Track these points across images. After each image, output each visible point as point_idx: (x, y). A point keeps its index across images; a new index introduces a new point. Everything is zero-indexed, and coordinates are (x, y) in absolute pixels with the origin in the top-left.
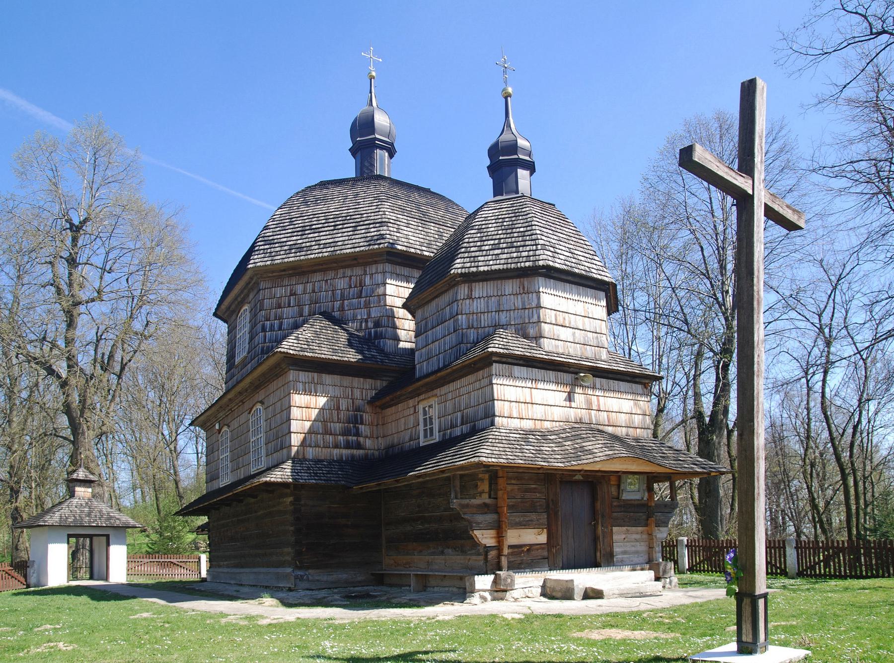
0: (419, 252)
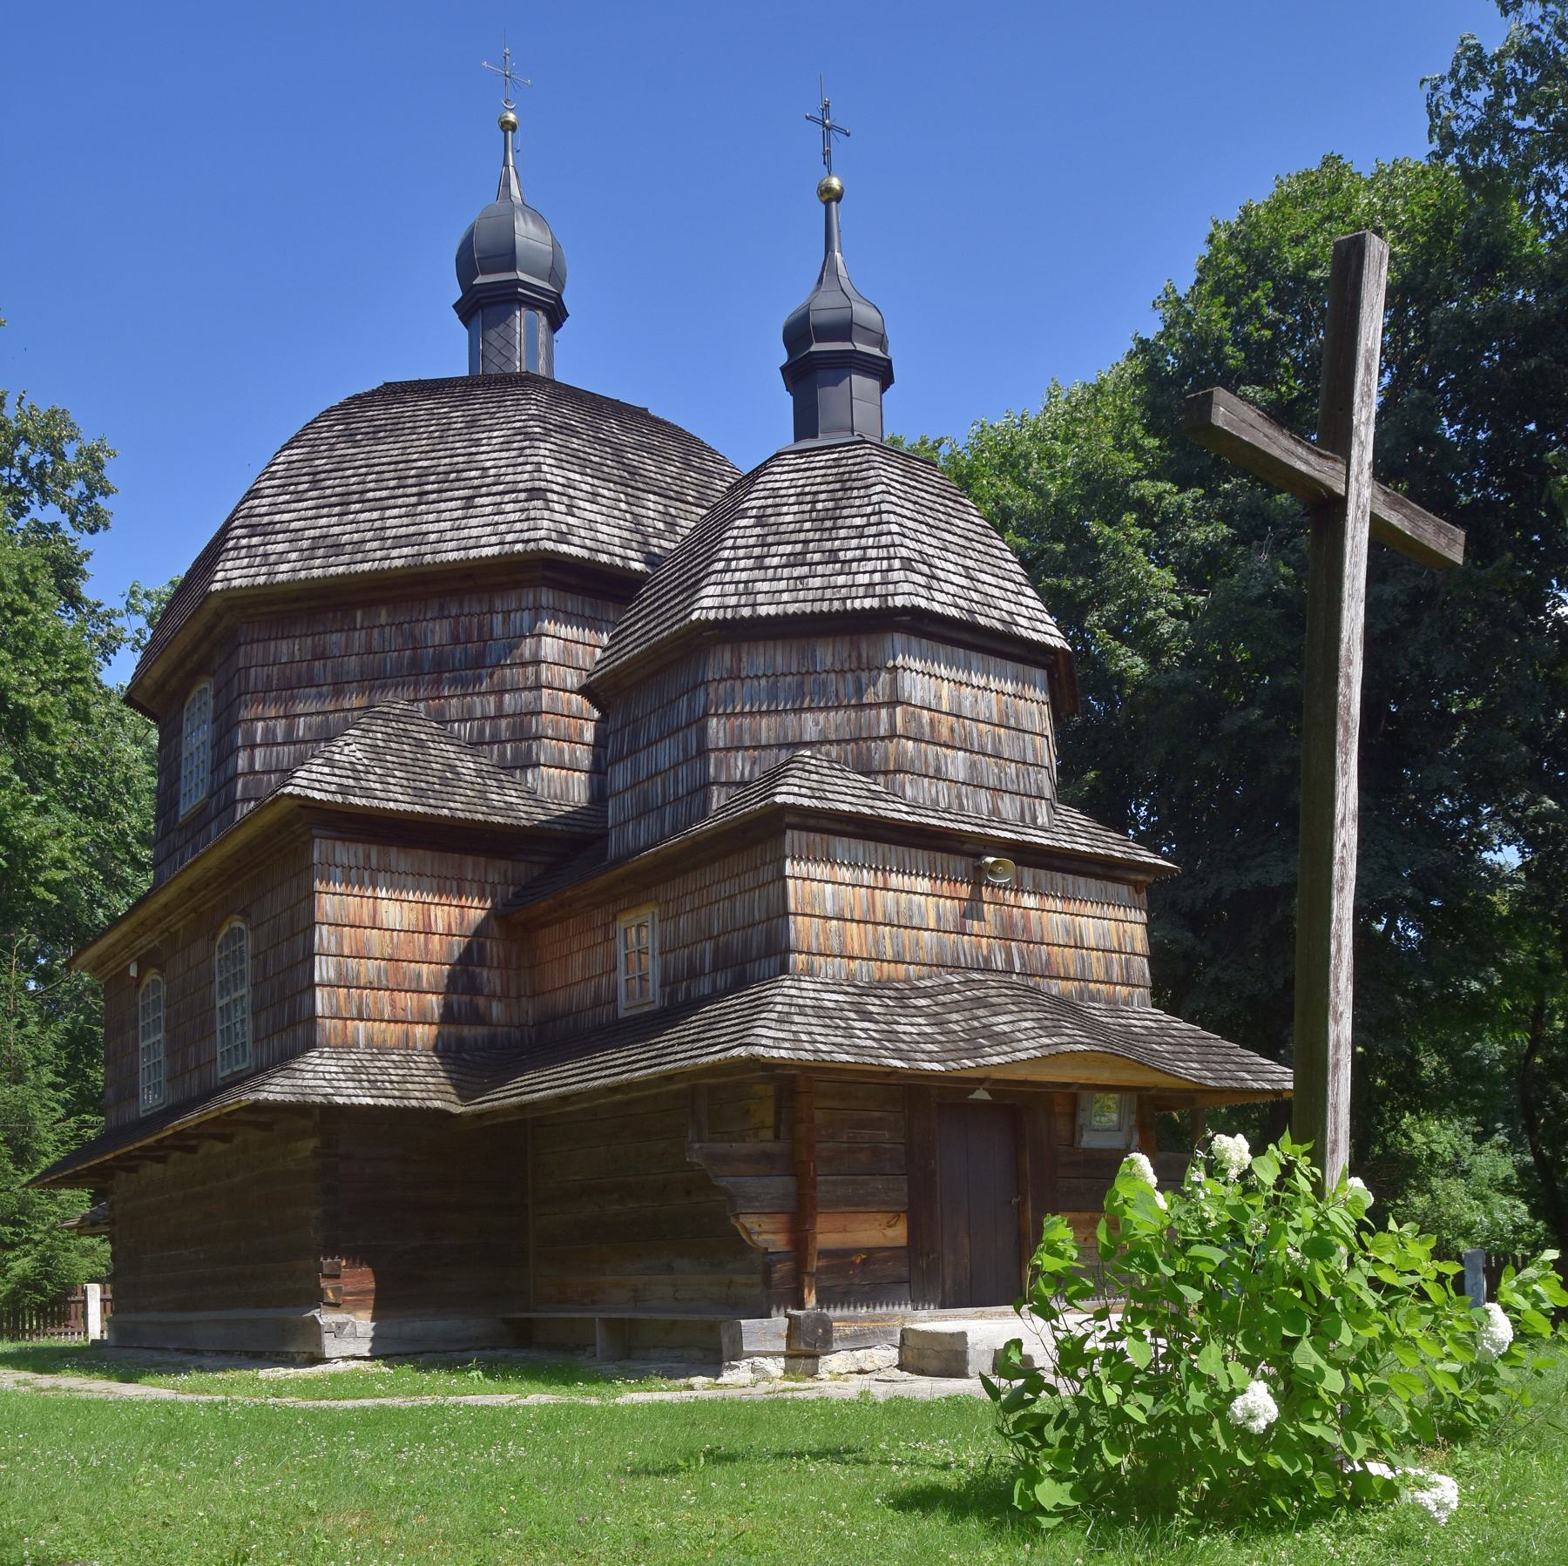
0: (618, 561)
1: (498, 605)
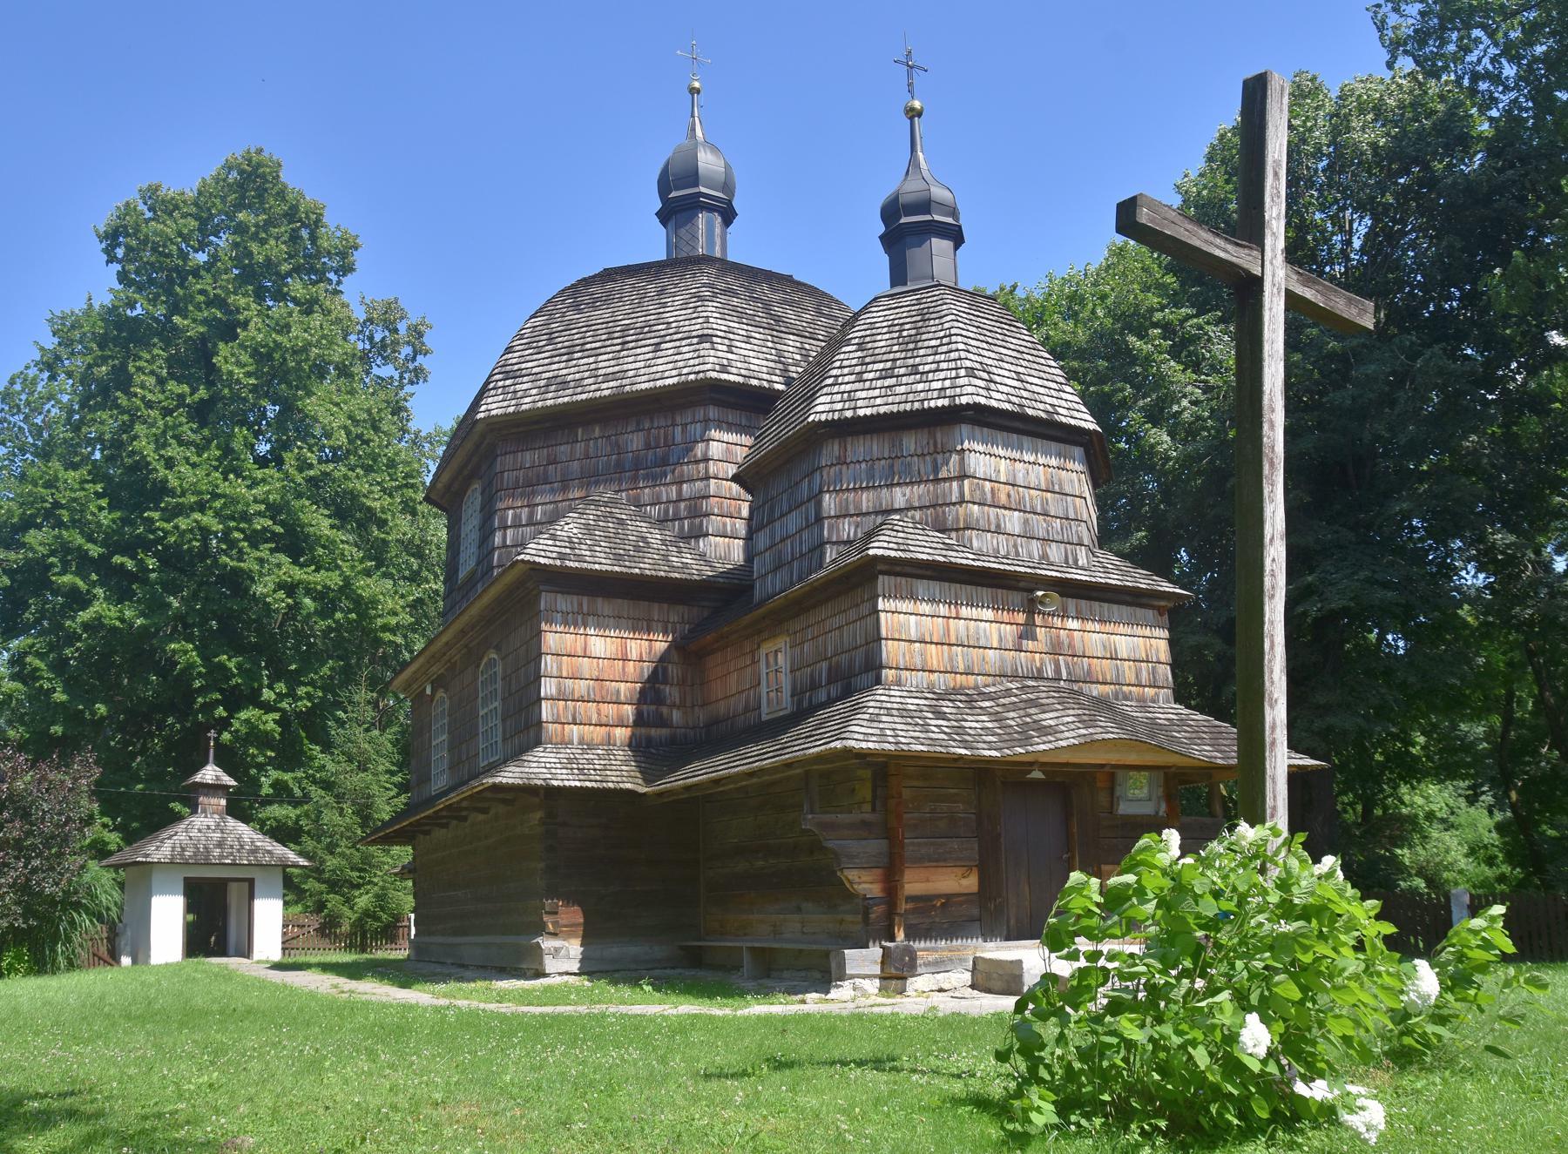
0: (765, 384)
1: (678, 420)
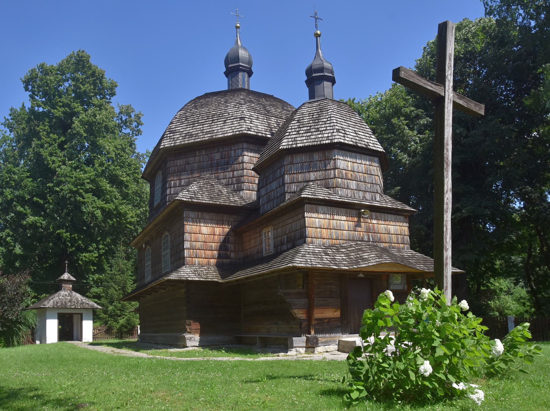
0: (264, 135)
1: (233, 148)
